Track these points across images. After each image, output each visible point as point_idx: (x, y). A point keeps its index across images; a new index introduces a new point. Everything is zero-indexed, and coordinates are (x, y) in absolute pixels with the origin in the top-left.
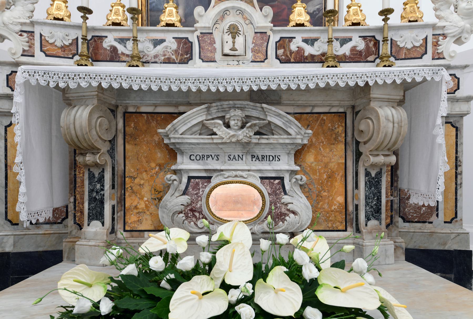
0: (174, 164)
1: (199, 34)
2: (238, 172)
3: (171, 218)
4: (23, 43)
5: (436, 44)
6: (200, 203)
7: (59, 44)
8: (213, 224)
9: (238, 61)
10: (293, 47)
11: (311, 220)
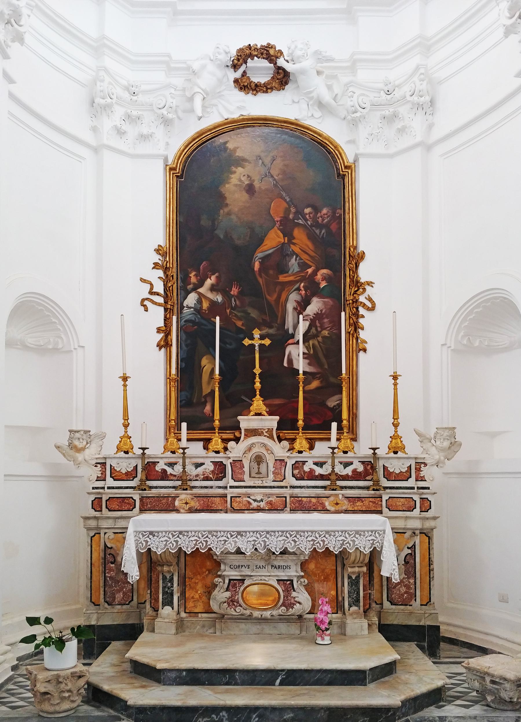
1: (232, 461)
4: (97, 472)
5: (418, 470)
6: (237, 596)
7: (124, 471)
9: (262, 481)
10: (306, 468)
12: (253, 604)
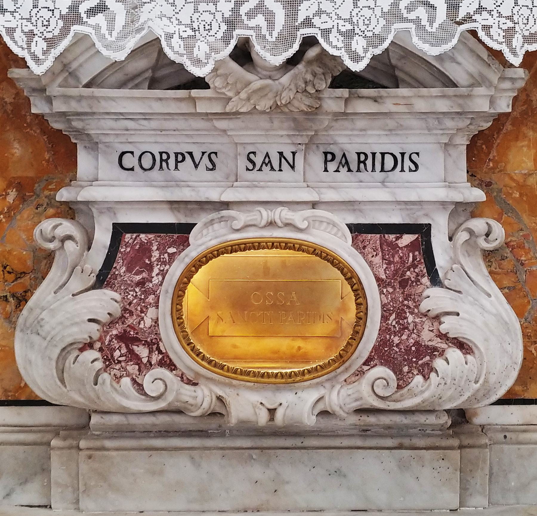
0: (67, 181)
2: (280, 209)
3: (54, 364)
6: (151, 312)
8: (195, 384)
11: (518, 368)
12: (237, 358)
